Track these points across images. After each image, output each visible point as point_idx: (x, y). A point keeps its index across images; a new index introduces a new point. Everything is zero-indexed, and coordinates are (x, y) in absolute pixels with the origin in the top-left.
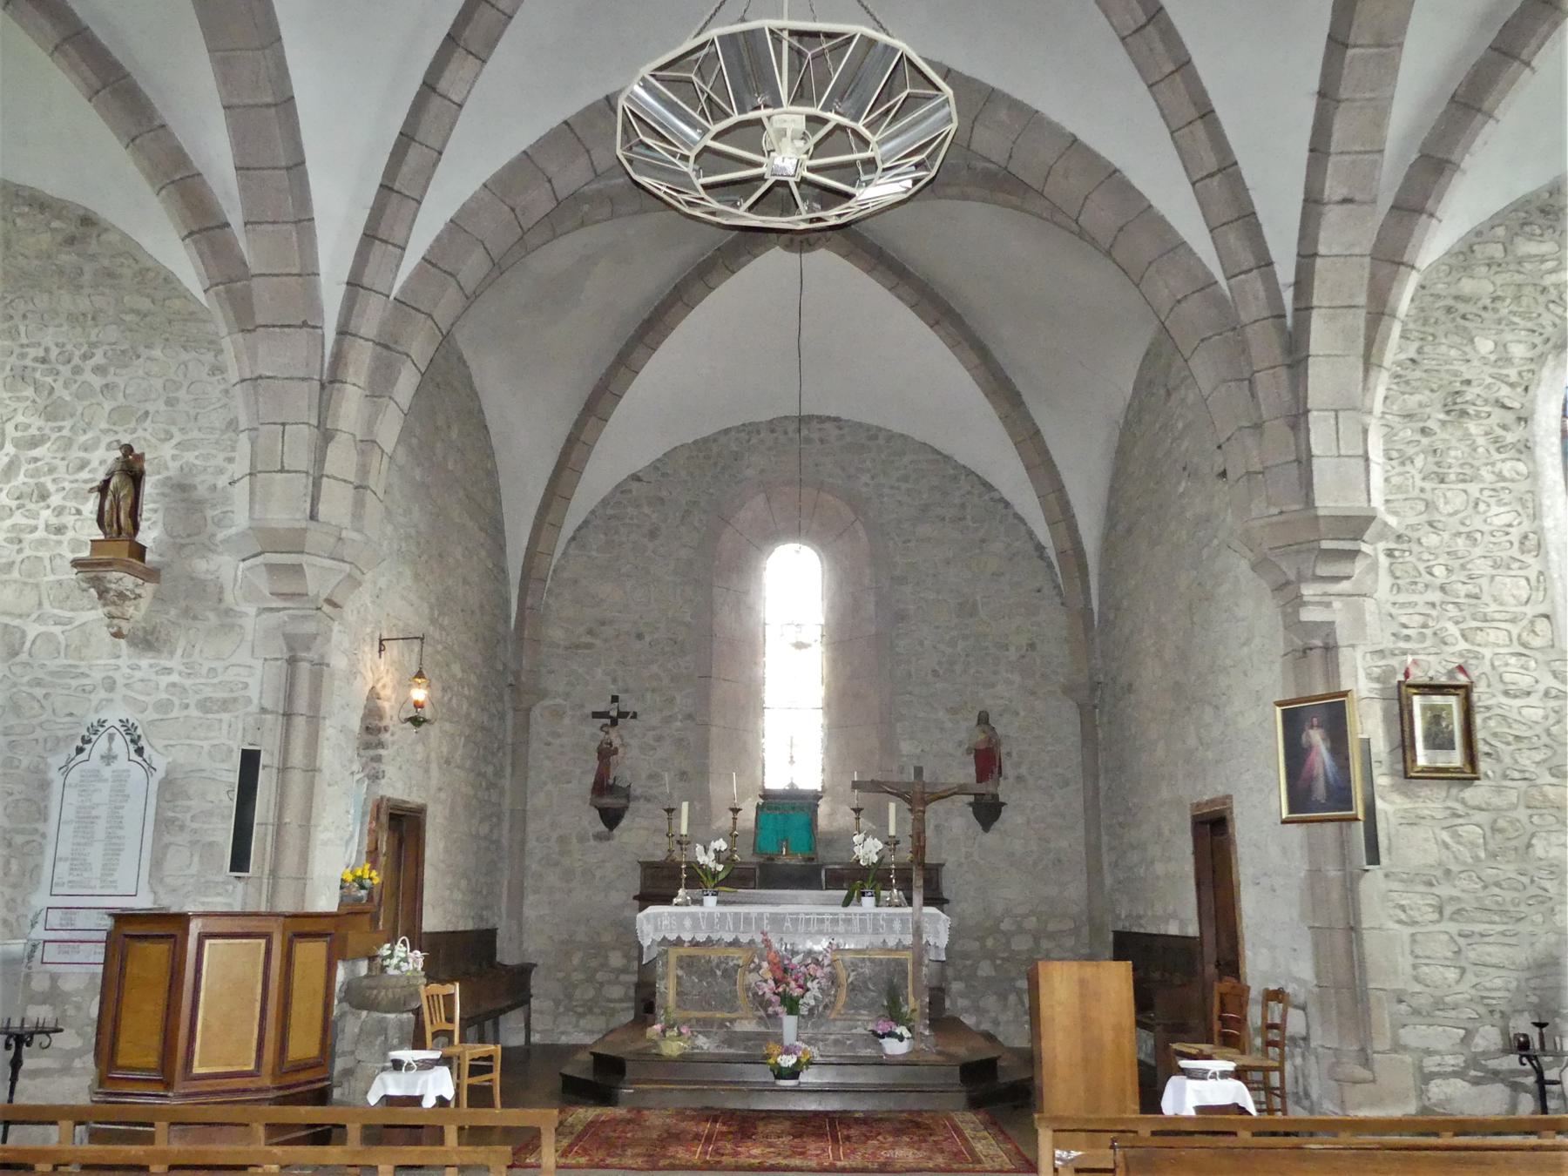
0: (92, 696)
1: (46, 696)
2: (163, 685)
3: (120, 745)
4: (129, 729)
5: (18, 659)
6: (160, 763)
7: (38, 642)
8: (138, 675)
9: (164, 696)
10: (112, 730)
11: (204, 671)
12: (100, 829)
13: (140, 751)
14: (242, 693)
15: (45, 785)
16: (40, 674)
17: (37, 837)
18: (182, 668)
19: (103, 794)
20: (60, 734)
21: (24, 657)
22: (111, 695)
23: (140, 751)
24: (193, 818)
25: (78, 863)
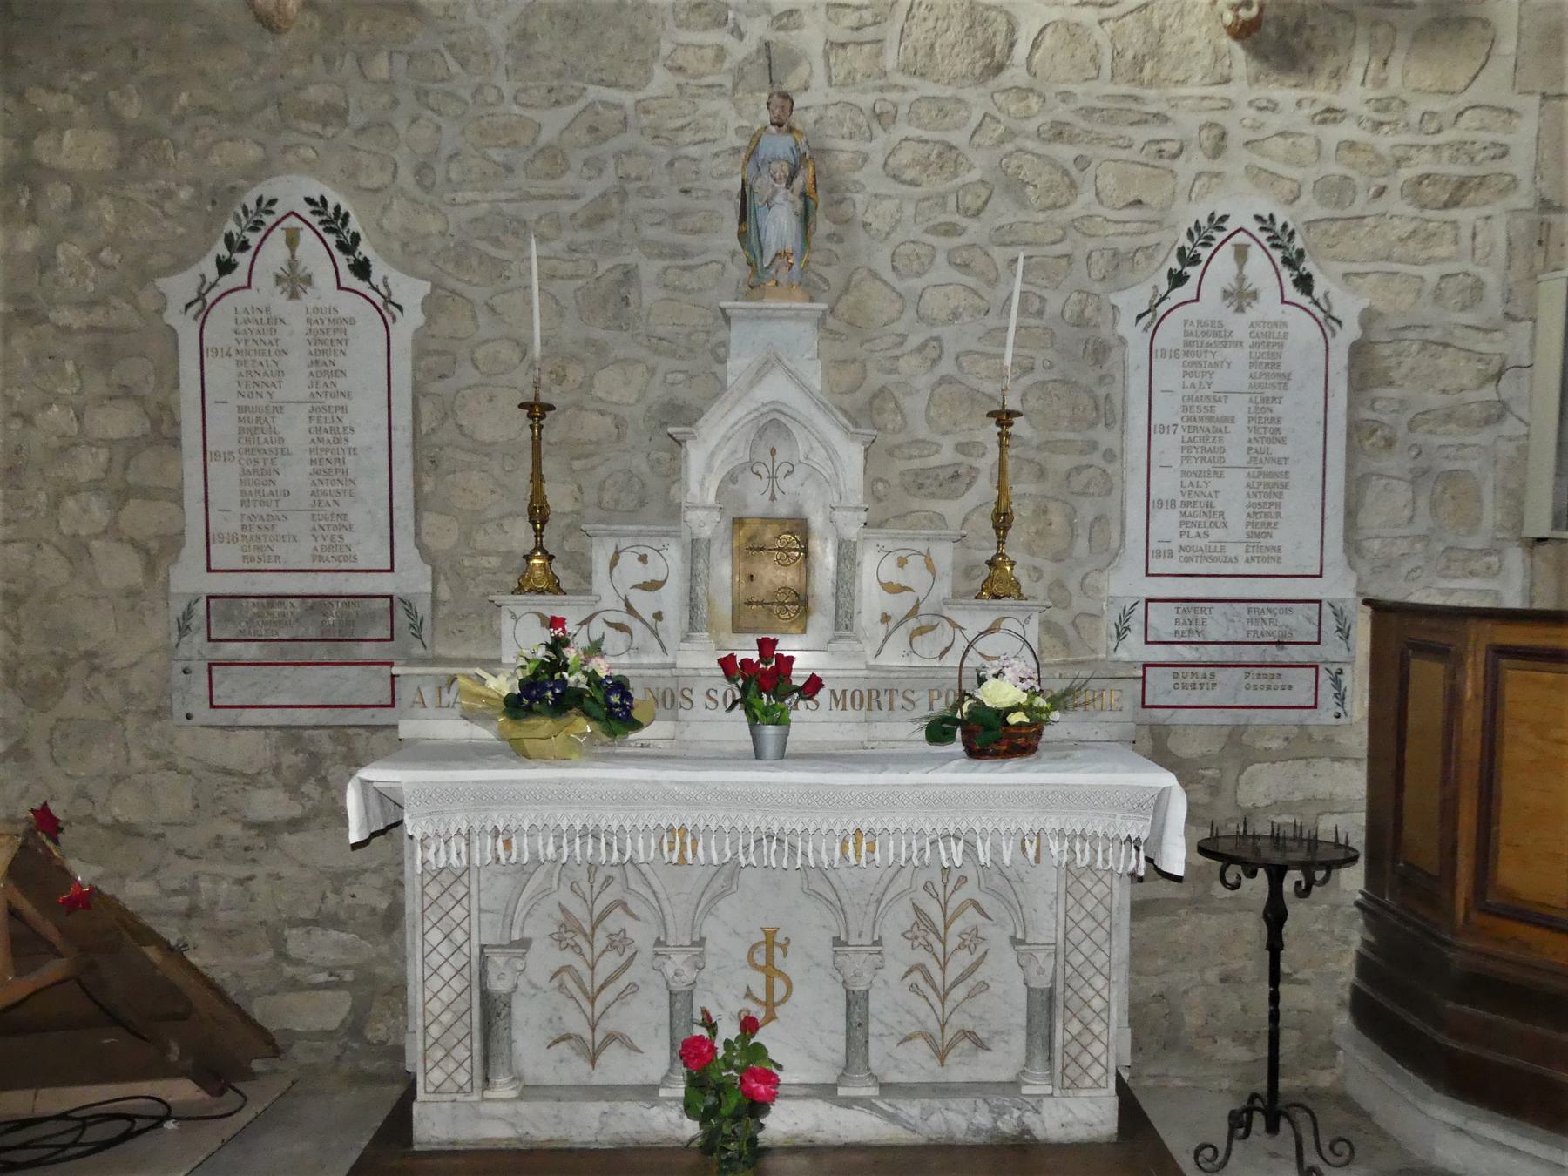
0: (1178, 165)
1: (1082, 162)
2: (1330, 145)
3: (1261, 268)
4: (1277, 236)
5: (1005, 79)
6: (1348, 307)
7: (1048, 41)
8: (1274, 122)
9: (1336, 169)
10: (1241, 238)
11: (1415, 117)
12: (1237, 441)
13: (1304, 283)
14: (1497, 166)
15: (1099, 352)
16: (1062, 112)
17: (1096, 459)
18: (1366, 111)
19: (1235, 370)
20: (1123, 244)
21: (1016, 74)
22: (1215, 166)
23: (1304, 283)
24: (1411, 426)
25: (1200, 512)
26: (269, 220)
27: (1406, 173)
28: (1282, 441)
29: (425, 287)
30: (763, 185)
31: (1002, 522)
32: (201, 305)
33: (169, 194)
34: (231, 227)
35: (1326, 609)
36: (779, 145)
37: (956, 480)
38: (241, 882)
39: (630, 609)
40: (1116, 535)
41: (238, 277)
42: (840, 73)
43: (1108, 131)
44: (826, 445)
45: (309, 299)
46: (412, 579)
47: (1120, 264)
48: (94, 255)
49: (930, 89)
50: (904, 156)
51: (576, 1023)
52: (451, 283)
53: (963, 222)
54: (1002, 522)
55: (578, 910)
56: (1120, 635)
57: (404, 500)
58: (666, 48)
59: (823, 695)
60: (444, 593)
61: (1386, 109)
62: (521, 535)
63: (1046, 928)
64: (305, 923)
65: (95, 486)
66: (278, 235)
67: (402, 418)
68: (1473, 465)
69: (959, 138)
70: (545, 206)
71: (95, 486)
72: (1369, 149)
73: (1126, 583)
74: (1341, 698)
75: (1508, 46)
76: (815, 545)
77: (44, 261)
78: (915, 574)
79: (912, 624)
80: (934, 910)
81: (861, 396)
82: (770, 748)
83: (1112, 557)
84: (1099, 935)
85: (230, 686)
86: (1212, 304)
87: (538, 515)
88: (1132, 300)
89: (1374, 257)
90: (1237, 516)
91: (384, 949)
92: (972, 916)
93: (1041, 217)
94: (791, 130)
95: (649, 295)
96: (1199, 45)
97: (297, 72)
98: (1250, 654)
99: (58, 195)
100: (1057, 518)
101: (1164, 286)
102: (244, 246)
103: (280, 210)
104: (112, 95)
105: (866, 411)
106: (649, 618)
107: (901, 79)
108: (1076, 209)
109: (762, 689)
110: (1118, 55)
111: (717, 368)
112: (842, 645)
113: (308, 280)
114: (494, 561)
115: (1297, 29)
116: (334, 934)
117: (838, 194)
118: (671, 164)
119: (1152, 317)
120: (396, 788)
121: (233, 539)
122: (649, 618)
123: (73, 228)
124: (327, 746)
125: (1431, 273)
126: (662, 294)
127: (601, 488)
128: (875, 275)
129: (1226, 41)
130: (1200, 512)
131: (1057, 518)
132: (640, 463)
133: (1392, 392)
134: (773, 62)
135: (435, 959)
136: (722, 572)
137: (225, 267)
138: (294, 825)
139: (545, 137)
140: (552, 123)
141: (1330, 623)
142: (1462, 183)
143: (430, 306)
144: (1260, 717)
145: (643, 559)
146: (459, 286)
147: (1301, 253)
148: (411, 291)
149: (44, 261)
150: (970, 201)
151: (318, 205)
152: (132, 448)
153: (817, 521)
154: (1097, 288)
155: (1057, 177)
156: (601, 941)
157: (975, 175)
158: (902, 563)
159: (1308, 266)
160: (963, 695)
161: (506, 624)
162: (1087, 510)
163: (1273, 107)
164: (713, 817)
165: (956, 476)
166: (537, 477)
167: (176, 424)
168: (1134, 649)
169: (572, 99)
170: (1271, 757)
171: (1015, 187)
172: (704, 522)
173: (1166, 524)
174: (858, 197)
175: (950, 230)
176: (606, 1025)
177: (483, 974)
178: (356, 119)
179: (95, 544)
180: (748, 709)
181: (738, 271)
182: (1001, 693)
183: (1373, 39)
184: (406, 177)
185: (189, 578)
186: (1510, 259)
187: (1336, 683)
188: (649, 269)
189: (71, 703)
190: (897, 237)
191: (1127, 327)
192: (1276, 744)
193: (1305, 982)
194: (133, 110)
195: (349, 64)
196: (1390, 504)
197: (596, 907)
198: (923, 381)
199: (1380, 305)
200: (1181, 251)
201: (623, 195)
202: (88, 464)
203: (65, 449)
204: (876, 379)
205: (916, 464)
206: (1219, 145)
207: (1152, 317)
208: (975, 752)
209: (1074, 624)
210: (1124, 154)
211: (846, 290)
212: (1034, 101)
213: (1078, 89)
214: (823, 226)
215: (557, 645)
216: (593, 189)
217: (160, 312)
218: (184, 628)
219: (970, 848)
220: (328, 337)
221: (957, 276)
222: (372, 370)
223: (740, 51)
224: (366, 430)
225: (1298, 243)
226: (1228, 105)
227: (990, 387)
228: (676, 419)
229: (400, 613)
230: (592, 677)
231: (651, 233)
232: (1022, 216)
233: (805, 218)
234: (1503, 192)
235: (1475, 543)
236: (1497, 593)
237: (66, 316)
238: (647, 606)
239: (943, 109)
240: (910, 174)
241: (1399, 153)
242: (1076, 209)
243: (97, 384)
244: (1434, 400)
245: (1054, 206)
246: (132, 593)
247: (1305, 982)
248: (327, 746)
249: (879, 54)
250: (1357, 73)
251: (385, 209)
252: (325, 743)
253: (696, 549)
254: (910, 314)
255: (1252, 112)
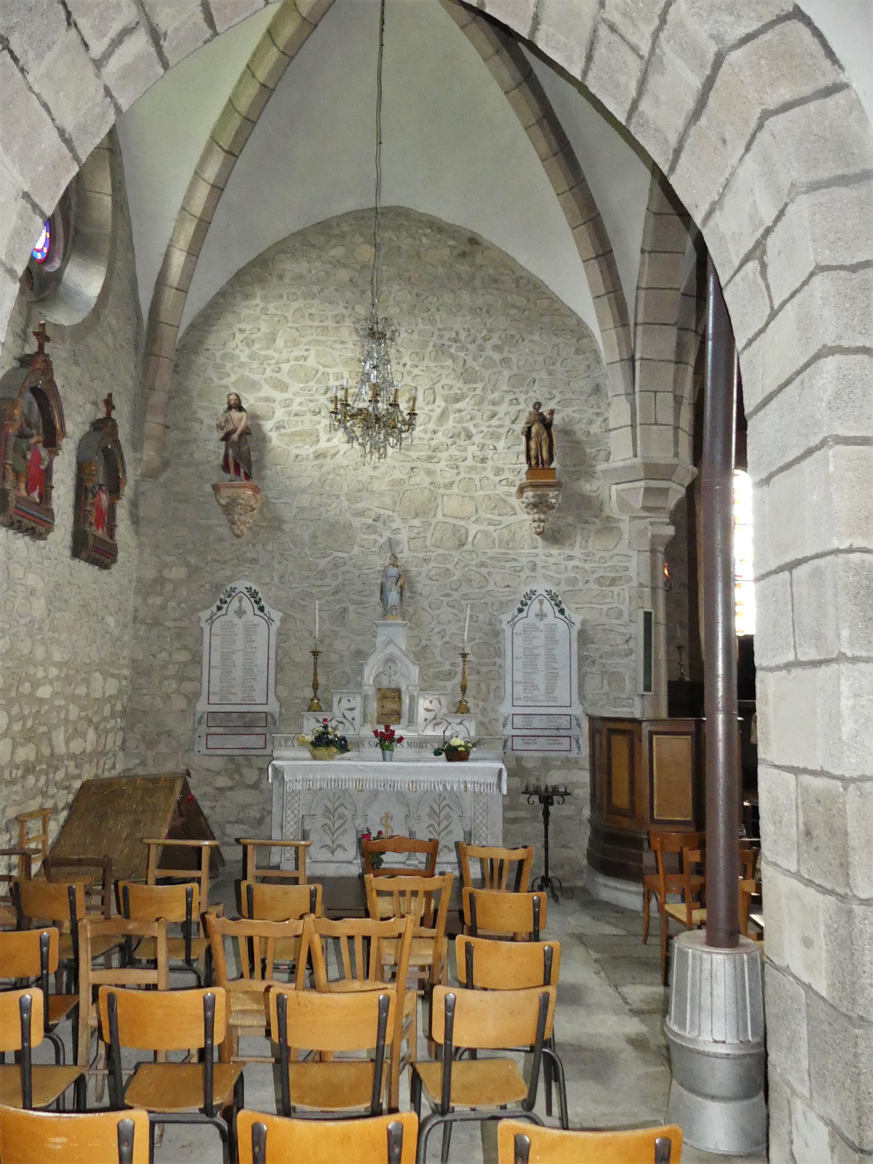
0: (521, 574)
1: (489, 573)
3: (547, 607)
4: (553, 597)
5: (466, 548)
6: (577, 619)
7: (479, 536)
8: (552, 560)
10: (541, 597)
11: (597, 558)
13: (562, 611)
16: (484, 558)
17: (496, 668)
18: (581, 556)
19: (540, 640)
20: (504, 599)
22: (533, 574)
23: (562, 611)
24: (601, 657)
25: (528, 684)
26: (233, 594)
27: (595, 576)
28: (556, 662)
29: (281, 614)
30: (388, 584)
31: (464, 689)
32: (211, 620)
33: (203, 586)
34: (222, 597)
35: (573, 718)
36: (394, 571)
37: (450, 675)
38: (211, 808)
39: (344, 717)
40: (503, 693)
41: (223, 612)
42: (413, 547)
43: (498, 564)
44: (407, 667)
45: (244, 618)
46: (273, 707)
47: (503, 606)
48: (179, 604)
49: (441, 551)
50: (433, 572)
51: (328, 842)
52: (288, 612)
53: (451, 592)
54: (464, 689)
55: (329, 805)
56: (504, 726)
57: (272, 682)
58: (358, 540)
59: (404, 742)
60: (283, 711)
61: (588, 556)
62: (309, 693)
63: (469, 813)
64: (232, 822)
65: (174, 677)
66: (237, 598)
67: (273, 655)
68: (622, 670)
69: (450, 566)
70: (319, 589)
71: (174, 677)
72: (583, 568)
73: (506, 709)
74: (579, 748)
75: (626, 536)
76: (403, 696)
77: (163, 607)
78: (435, 705)
79: (434, 722)
80: (436, 807)
81: (419, 648)
82: (388, 758)
83: (502, 700)
84: (485, 814)
85: (213, 742)
86: (532, 619)
87: (315, 686)
88: (506, 617)
89: (586, 603)
90: (542, 687)
91: (257, 832)
92: (447, 809)
93: (477, 591)
94: (397, 566)
95: (352, 616)
96: (527, 537)
97: (244, 549)
98: (548, 733)
99: (169, 587)
100: (483, 687)
101: (516, 613)
102: (226, 602)
103: (237, 591)
104: (188, 557)
105: (420, 654)
106: (350, 719)
107: (432, 549)
108: (489, 588)
109: (386, 740)
110: (500, 541)
111: (373, 639)
112: (411, 728)
113: (245, 612)
114: (300, 701)
115: (558, 532)
116: (242, 826)
117: (411, 584)
118: (359, 576)
119: (513, 622)
120: (282, 766)
121: (216, 694)
122: (350, 719)
123: (173, 597)
124: (243, 762)
125: (605, 607)
126: (356, 616)
127: (335, 676)
128: (423, 609)
129: (535, 536)
130: (528, 684)
131: (483, 687)
132: (348, 670)
133: (594, 646)
134: (391, 544)
135: (289, 819)
136: (374, 706)
137: (219, 608)
138: (231, 788)
139: (320, 567)
140: (323, 563)
141: (574, 722)
142: (614, 579)
143: (283, 620)
144: (552, 754)
145: (349, 701)
146: (292, 614)
147: (560, 602)
148: (276, 615)
149: (163, 607)
150: (454, 586)
151: (249, 589)
152: (186, 664)
153: (403, 689)
154: (495, 613)
155: (482, 578)
156: (337, 815)
157: (455, 578)
158: (431, 702)
159: (563, 606)
160: (445, 743)
161: (305, 722)
162: (493, 685)
163: (551, 555)
164: (371, 776)
165: (450, 673)
166: (315, 674)
167: (201, 657)
168: (509, 731)
169: (328, 556)
170: (557, 768)
171: (469, 581)
172: (370, 691)
173: (519, 689)
174: (418, 585)
175: (447, 595)
176: (339, 842)
177: (303, 822)
178: (261, 563)
179: (172, 695)
180: (381, 746)
181: (380, 609)
182: (456, 742)
183: (582, 535)
184: (276, 579)
185: (202, 707)
186: (630, 602)
187: (577, 742)
188: (352, 608)
189: (161, 748)
190: (431, 597)
191: (504, 626)
192: (559, 763)
193: (572, 848)
194: (193, 561)
195: (260, 546)
196: (593, 683)
197: (335, 803)
198: (439, 643)
199: (588, 618)
200: (522, 602)
201: (344, 585)
202: (172, 670)
203: (165, 667)
204: (424, 642)
205: (438, 670)
206: (534, 567)
207: (513, 622)
208: (449, 759)
209: (490, 723)
210: (503, 571)
211: (415, 614)
212: (474, 555)
213: (488, 551)
214: (407, 594)
215: (326, 727)
216: (336, 583)
217: (199, 621)
218: (200, 723)
219: (445, 786)
220: (250, 629)
221: (450, 609)
222: (264, 638)
223: (381, 541)
224: (261, 659)
225: (560, 598)
226: (537, 555)
227: (461, 645)
228: (360, 656)
229: (269, 718)
230: (336, 736)
231: (353, 597)
232: (472, 590)
233: (401, 593)
234: (628, 581)
235: (624, 696)
236: (632, 712)
237: (168, 624)
238: (352, 714)
239: (445, 558)
240: (434, 578)
241: (593, 569)
242: (489, 588)
243: (177, 645)
244: (608, 648)
245: (481, 587)
246: (182, 711)
247: (572, 848)
248: (243, 762)
249: (426, 541)
250: (578, 544)
251: (270, 589)
252: (242, 760)
253: (366, 698)
254: (434, 622)
255: (544, 557)
